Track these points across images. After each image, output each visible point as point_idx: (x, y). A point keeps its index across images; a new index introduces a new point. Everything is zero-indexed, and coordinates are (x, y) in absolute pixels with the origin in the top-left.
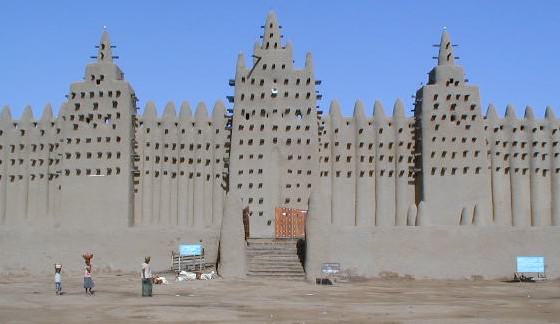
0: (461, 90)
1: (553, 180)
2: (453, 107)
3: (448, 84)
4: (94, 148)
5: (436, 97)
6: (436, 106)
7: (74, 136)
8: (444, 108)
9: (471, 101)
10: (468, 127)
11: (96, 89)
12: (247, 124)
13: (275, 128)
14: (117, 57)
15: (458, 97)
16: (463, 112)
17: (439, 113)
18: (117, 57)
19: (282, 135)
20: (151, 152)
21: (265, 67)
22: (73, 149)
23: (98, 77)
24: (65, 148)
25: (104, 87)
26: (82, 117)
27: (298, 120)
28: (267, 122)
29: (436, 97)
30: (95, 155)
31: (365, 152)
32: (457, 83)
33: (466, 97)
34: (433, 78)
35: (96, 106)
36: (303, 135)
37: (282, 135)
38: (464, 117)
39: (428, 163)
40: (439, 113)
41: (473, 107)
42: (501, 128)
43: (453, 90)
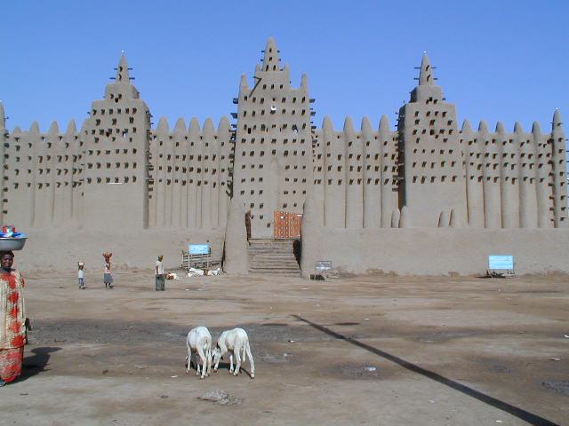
0: (440, 108)
1: (521, 187)
2: (432, 122)
3: (427, 102)
4: (113, 159)
6: (417, 122)
7: (95, 148)
9: (448, 117)
10: (445, 140)
11: (115, 106)
12: (249, 137)
13: (274, 141)
15: (436, 113)
16: (440, 127)
17: (419, 128)
19: (280, 147)
20: (163, 162)
21: (265, 87)
22: (94, 159)
23: (116, 96)
24: (87, 159)
25: (122, 105)
26: (102, 132)
27: (295, 134)
30: (114, 165)
31: (354, 162)
32: (435, 101)
33: (444, 114)
34: (414, 96)
35: (115, 121)
36: (299, 148)
37: (280, 147)
38: (442, 131)
39: (410, 173)
40: (419, 128)
43: (432, 107)
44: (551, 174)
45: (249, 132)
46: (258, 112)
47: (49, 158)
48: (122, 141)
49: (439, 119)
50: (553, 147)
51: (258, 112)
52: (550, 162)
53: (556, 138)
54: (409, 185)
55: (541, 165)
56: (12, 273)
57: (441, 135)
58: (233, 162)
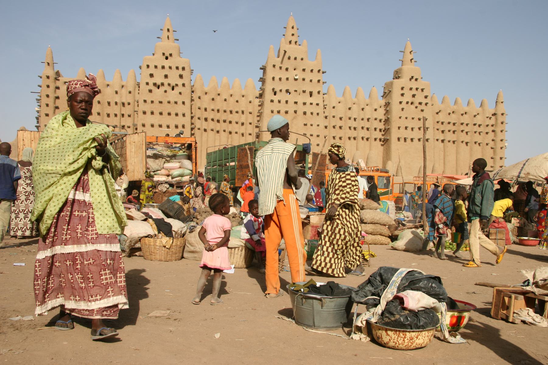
0: (420, 84)
1: (471, 149)
2: (414, 96)
3: (410, 80)
4: (166, 108)
5: (402, 88)
6: (402, 95)
7: (149, 98)
8: (408, 97)
9: (425, 93)
10: (422, 111)
11: (167, 64)
13: (296, 103)
14: (178, 40)
15: (417, 89)
16: (419, 100)
17: (404, 100)
18: (178, 40)
19: (301, 109)
21: (289, 58)
22: (148, 108)
24: (143, 107)
26: (155, 84)
28: (291, 98)
29: (402, 88)
30: (165, 113)
32: (416, 80)
33: (422, 90)
34: (397, 75)
35: (166, 76)
36: (315, 110)
37: (301, 109)
38: (420, 103)
39: (394, 134)
40: (404, 100)
41: (177, 68)
42: (453, 112)
43: (414, 84)
44: (493, 140)
45: (167, 58)
46: (284, 79)
47: (144, 113)
48: (173, 95)
49: (419, 94)
50: (496, 119)
51: (284, 79)
52: (493, 131)
53: (499, 113)
54: (394, 144)
55: (487, 133)
56: (518, 225)
57: (419, 106)
58: (192, 97)
